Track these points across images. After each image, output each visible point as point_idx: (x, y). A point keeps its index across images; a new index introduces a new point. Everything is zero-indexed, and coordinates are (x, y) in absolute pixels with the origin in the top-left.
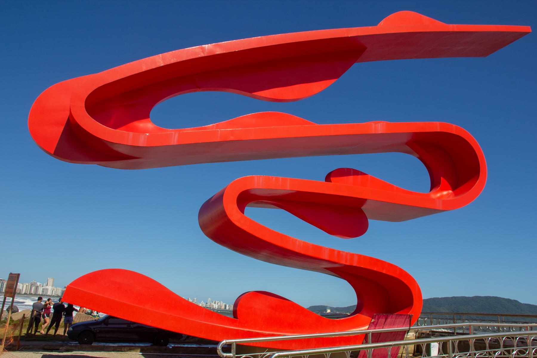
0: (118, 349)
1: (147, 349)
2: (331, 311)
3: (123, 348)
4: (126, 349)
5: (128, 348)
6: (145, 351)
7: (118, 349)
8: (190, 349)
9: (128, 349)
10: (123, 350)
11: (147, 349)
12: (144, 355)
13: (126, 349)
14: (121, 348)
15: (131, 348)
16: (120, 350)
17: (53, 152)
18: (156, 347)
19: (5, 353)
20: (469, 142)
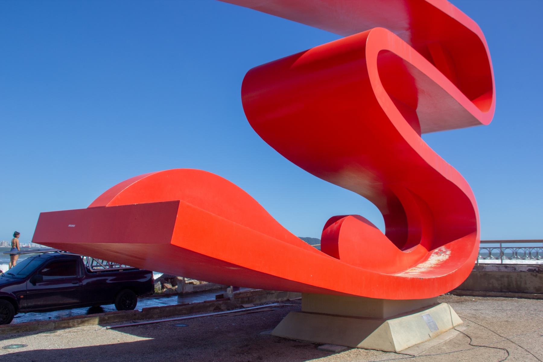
0: (63, 325)
1: (108, 317)
2: (232, 286)
3: (71, 321)
4: (76, 321)
5: (79, 320)
6: (105, 322)
7: (63, 325)
8: (167, 309)
9: (79, 322)
10: (71, 324)
11: (108, 317)
12: (121, 329)
13: (76, 321)
14: (68, 323)
15: (84, 319)
16: (67, 325)
17: (151, 274)
18: (122, 313)
19: (97, 325)
20: (155, 202)
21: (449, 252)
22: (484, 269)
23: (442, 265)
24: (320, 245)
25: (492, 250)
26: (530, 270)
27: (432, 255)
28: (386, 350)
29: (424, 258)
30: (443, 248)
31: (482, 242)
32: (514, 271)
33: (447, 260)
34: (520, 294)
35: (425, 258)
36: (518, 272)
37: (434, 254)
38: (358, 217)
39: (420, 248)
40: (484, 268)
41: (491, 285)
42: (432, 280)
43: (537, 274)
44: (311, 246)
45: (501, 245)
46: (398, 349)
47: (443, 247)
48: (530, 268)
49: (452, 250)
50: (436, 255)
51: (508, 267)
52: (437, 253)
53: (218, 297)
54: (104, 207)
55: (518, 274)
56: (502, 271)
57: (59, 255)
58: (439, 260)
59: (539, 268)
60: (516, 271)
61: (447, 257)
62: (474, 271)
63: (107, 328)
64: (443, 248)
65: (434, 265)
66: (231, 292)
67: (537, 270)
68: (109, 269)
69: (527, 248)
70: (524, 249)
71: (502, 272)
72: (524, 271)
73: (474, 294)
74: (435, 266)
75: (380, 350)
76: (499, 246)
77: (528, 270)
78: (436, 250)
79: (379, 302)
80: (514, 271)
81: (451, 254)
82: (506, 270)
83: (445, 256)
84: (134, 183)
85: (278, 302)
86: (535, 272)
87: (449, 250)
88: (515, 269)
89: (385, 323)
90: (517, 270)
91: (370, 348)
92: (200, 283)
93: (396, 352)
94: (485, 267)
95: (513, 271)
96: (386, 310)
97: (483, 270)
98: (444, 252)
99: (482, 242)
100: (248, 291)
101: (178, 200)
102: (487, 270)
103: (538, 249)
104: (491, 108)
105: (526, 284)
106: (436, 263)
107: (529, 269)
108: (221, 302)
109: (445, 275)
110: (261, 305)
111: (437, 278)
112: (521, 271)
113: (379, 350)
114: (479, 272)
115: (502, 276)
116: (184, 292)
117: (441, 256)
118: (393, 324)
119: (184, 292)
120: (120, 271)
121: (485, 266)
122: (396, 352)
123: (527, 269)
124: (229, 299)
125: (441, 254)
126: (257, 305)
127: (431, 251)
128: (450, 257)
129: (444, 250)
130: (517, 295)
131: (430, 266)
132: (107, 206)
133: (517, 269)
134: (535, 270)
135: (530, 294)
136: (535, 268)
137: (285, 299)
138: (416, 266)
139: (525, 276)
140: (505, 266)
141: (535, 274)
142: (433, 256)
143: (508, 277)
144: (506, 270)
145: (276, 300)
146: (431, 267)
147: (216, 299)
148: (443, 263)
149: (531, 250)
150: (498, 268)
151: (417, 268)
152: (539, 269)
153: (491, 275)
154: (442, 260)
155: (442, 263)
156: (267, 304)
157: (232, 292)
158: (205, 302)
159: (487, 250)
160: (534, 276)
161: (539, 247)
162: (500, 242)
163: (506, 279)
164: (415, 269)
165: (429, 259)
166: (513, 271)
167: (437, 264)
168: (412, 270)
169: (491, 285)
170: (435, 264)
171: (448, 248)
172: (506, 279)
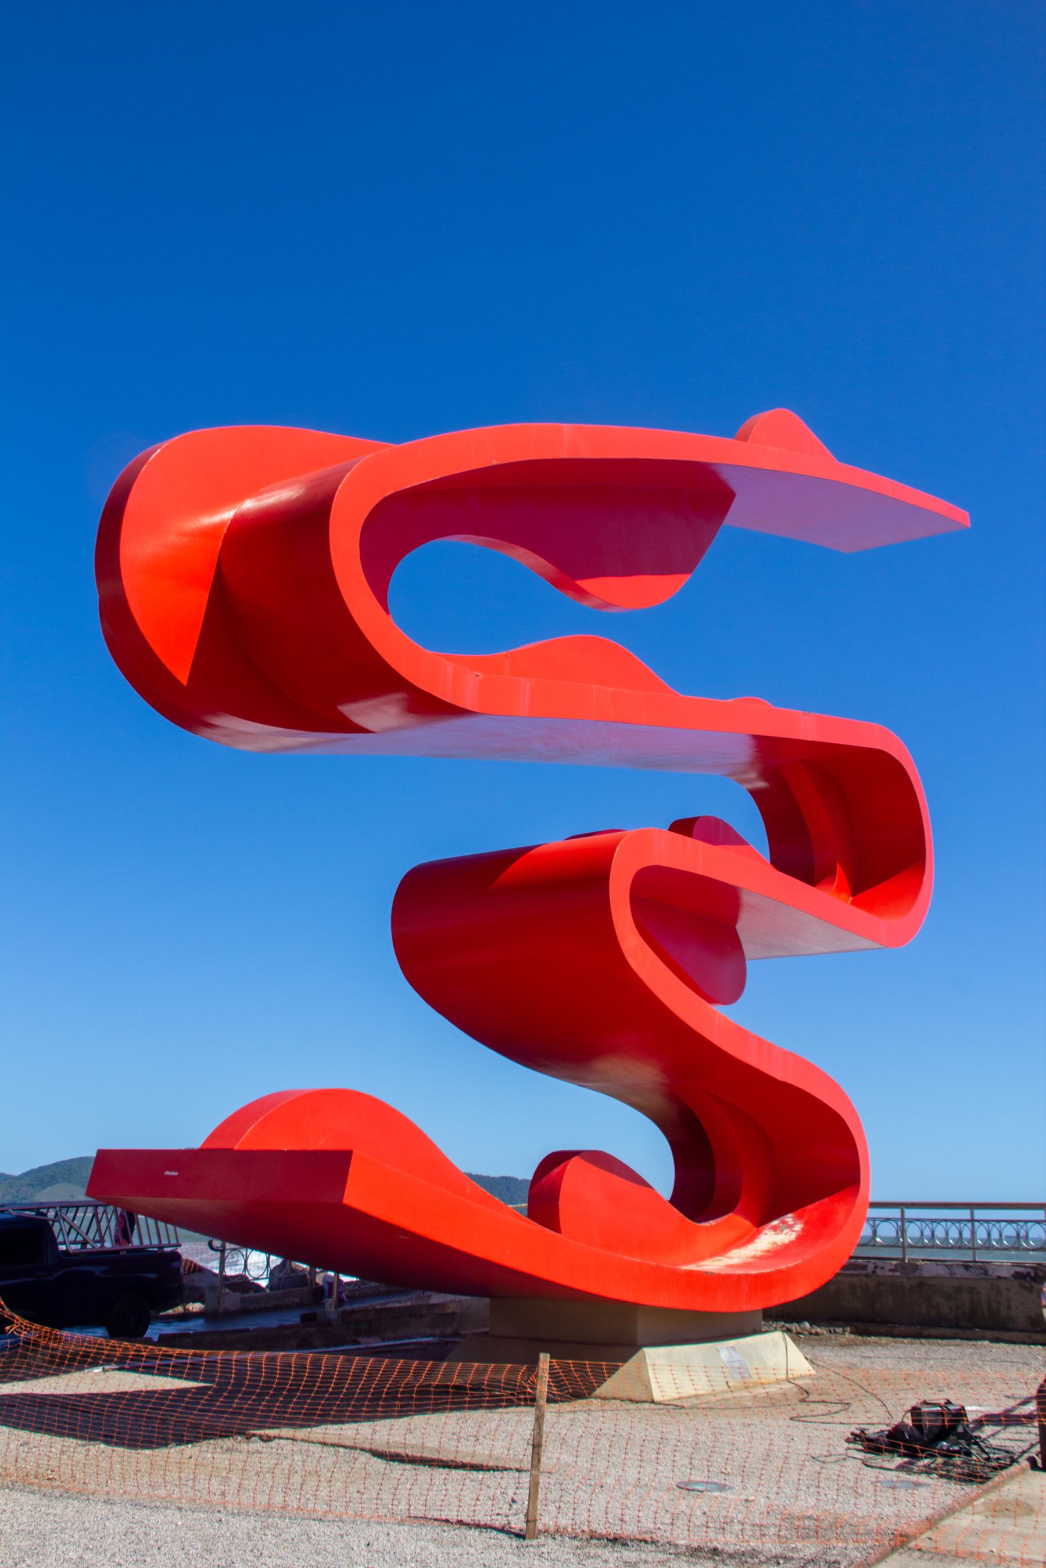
21: (798, 1227)
22: (918, 1271)
23: (778, 1252)
24: (526, 1205)
25: (1032, 1226)
26: (1017, 1275)
27: (765, 1231)
28: (637, 1398)
29: (748, 1237)
30: (789, 1218)
31: (874, 1205)
32: (985, 1277)
33: (792, 1243)
34: (995, 1334)
35: (748, 1238)
36: (993, 1279)
37: (770, 1229)
38: (600, 1160)
39: (735, 1220)
40: (918, 1269)
41: (933, 1312)
42: (735, 1278)
43: (1034, 1284)
44: (509, 1208)
45: (972, 1214)
46: (657, 1396)
47: (790, 1215)
48: (1018, 1269)
49: (806, 1223)
50: (773, 1233)
51: (971, 1266)
52: (775, 1228)
53: (304, 1318)
54: (232, 1149)
55: (992, 1285)
56: (959, 1276)
57: (9, 1219)
58: (776, 1243)
59: (1037, 1271)
60: (988, 1277)
61: (793, 1236)
62: (897, 1277)
63: (104, 1368)
64: (789, 1218)
65: (762, 1252)
66: (333, 1309)
67: (1032, 1274)
68: (100, 1250)
69: (1021, 1224)
70: (919, 1223)
71: (957, 1279)
72: (1005, 1278)
73: (896, 1331)
74: (764, 1254)
75: (627, 1400)
76: (968, 1217)
77: (1013, 1276)
78: (775, 1223)
79: (628, 1309)
80: (985, 1277)
81: (803, 1230)
82: (966, 1274)
83: (790, 1235)
84: (265, 1116)
85: (434, 1336)
86: (1028, 1279)
87: (800, 1222)
88: (986, 1273)
89: (639, 1353)
90: (990, 1276)
91: (610, 1396)
92: (185, 1309)
93: (653, 1402)
94: (920, 1268)
95: (982, 1276)
96: (642, 1327)
97: (917, 1274)
98: (790, 1227)
99: (874, 1205)
100: (370, 1308)
101: (348, 1148)
102: (925, 1274)
103: (949, 1224)
104: (913, 909)
105: (1009, 1308)
106: (766, 1249)
107: (1016, 1273)
108: (312, 1330)
109: (768, 1270)
110: (395, 1339)
111: (747, 1276)
112: (999, 1277)
113: (625, 1399)
114: (908, 1278)
115: (959, 1290)
116: (221, 1310)
117: (781, 1233)
118: (653, 1355)
119: (221, 1310)
120: (121, 1253)
121: (921, 1265)
122: (653, 1402)
123: (1012, 1272)
124: (329, 1323)
125: (782, 1231)
126: (389, 1340)
127: (761, 1228)
128: (798, 1237)
129: (790, 1223)
130: (989, 1334)
131: (752, 1254)
132: (236, 1148)
133: (990, 1273)
134: (1028, 1274)
135: (1016, 1333)
136: (1029, 1270)
137: (450, 1330)
138: (726, 1253)
139: (1008, 1289)
140: (964, 1265)
141: (1028, 1285)
142: (766, 1234)
143: (971, 1290)
144: (966, 1274)
145: (428, 1331)
146: (755, 1257)
147: (302, 1321)
148: (780, 1250)
149: (1002, 1226)
150: (950, 1269)
151: (727, 1257)
152: (1036, 1273)
153: (934, 1286)
154: (780, 1244)
155: (779, 1248)
156: (410, 1338)
157: (336, 1308)
158: (281, 1327)
159: (1030, 1228)
160: (1025, 1288)
161: (951, 1221)
162: (902, 1205)
163: (966, 1296)
164: (719, 1260)
165: (757, 1240)
166: (982, 1276)
167: (768, 1251)
168: (714, 1261)
169: (933, 1312)
170: (765, 1251)
171: (799, 1217)
172: (966, 1296)
